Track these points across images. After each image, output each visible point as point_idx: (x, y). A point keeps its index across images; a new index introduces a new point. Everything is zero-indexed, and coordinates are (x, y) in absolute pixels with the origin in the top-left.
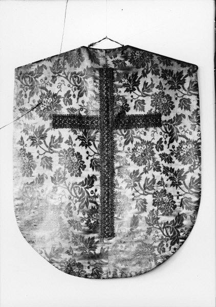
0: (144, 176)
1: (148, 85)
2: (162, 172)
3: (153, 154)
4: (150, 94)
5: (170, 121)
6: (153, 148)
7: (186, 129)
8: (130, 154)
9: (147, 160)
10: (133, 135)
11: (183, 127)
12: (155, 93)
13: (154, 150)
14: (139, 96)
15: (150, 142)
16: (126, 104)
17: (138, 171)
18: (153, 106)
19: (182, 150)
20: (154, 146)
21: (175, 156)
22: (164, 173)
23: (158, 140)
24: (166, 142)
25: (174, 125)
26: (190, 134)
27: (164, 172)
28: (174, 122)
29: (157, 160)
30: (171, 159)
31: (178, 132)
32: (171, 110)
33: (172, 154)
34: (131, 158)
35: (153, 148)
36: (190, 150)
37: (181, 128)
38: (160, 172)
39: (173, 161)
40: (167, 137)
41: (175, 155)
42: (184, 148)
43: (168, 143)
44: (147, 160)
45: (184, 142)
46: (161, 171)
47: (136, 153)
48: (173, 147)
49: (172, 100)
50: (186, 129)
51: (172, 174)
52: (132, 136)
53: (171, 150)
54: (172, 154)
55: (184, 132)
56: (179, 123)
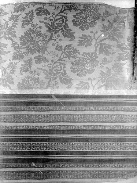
0: (9, 43)
1: (109, 50)
2: (13, 14)
3: (32, 52)
4: (98, 53)
5: (64, 73)
6: (39, 53)
7: (58, 40)
8: (33, 75)
9: (26, 46)
10: (54, 32)
11: (59, 38)
12: (97, 57)
13: (37, 54)
14: (96, 40)
15: (46, 50)
16: (86, 73)
17: (15, 36)
18: (83, 55)
19: (35, 83)
20: (41, 54)
21: (30, 29)
22: (11, 16)
23: (47, 58)
24: (44, 66)
25: (62, 29)
26: (53, 44)
27: (11, 63)
28: (66, 30)
29: (27, 8)
30: (27, 24)
31: (55, 33)
32: (77, 73)
33: (33, 26)
34: (30, 29)
35: (39, 53)
36: (37, 43)
37: (59, 36)
38: (13, 11)
39: (25, 26)
40: (51, 20)
41: (30, 75)
42: (39, 38)
43: (43, 68)
44: (26, 46)
45: (44, 85)
46: (14, 12)
47: (35, 34)
48: (38, 74)
49: (90, 28)
50: (58, 40)
51: (9, 72)
52: (53, 31)
53: (37, 25)
54: (33, 26)
55: (55, 38)
56: (65, 36)
